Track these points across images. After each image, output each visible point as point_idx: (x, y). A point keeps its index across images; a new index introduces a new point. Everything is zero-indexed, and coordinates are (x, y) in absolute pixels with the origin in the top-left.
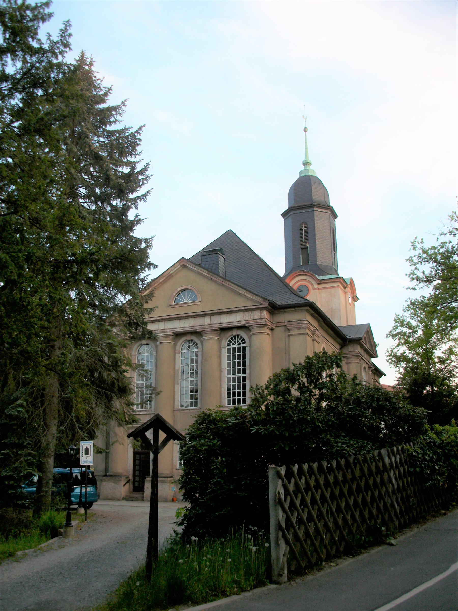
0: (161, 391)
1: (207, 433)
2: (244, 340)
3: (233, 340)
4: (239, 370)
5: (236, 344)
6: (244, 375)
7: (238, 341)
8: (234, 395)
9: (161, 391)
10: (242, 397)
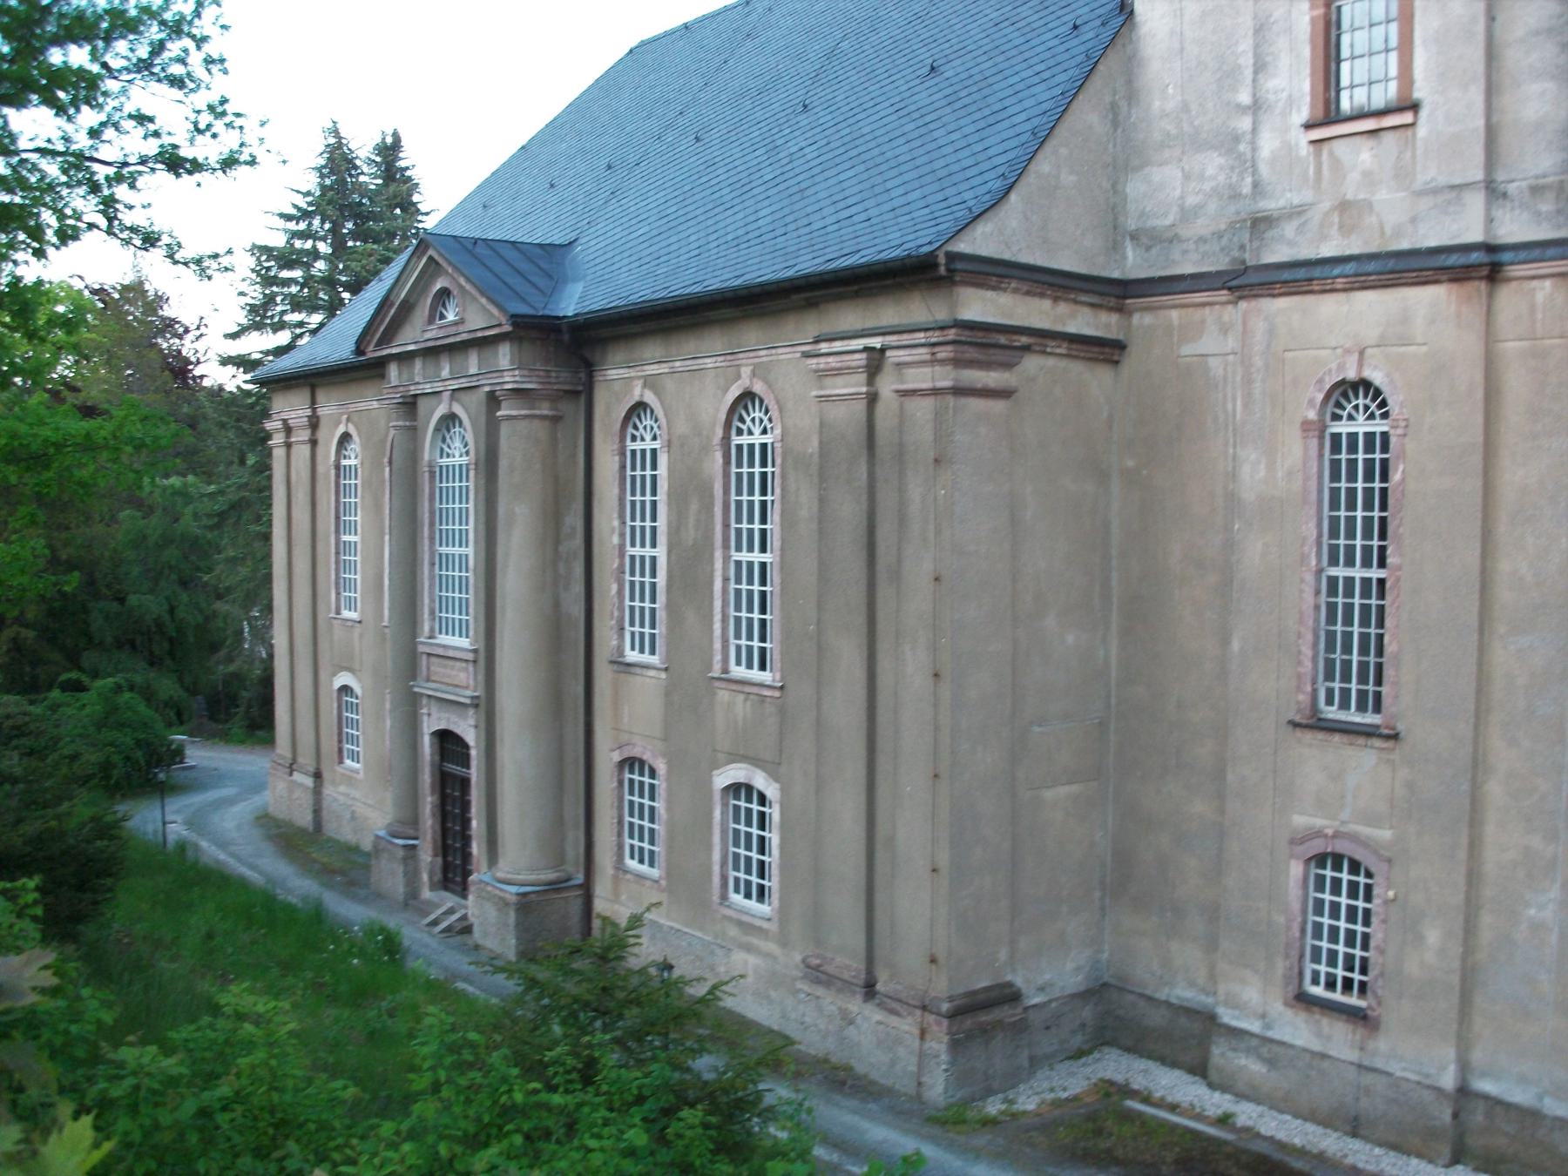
7: (1367, 408)
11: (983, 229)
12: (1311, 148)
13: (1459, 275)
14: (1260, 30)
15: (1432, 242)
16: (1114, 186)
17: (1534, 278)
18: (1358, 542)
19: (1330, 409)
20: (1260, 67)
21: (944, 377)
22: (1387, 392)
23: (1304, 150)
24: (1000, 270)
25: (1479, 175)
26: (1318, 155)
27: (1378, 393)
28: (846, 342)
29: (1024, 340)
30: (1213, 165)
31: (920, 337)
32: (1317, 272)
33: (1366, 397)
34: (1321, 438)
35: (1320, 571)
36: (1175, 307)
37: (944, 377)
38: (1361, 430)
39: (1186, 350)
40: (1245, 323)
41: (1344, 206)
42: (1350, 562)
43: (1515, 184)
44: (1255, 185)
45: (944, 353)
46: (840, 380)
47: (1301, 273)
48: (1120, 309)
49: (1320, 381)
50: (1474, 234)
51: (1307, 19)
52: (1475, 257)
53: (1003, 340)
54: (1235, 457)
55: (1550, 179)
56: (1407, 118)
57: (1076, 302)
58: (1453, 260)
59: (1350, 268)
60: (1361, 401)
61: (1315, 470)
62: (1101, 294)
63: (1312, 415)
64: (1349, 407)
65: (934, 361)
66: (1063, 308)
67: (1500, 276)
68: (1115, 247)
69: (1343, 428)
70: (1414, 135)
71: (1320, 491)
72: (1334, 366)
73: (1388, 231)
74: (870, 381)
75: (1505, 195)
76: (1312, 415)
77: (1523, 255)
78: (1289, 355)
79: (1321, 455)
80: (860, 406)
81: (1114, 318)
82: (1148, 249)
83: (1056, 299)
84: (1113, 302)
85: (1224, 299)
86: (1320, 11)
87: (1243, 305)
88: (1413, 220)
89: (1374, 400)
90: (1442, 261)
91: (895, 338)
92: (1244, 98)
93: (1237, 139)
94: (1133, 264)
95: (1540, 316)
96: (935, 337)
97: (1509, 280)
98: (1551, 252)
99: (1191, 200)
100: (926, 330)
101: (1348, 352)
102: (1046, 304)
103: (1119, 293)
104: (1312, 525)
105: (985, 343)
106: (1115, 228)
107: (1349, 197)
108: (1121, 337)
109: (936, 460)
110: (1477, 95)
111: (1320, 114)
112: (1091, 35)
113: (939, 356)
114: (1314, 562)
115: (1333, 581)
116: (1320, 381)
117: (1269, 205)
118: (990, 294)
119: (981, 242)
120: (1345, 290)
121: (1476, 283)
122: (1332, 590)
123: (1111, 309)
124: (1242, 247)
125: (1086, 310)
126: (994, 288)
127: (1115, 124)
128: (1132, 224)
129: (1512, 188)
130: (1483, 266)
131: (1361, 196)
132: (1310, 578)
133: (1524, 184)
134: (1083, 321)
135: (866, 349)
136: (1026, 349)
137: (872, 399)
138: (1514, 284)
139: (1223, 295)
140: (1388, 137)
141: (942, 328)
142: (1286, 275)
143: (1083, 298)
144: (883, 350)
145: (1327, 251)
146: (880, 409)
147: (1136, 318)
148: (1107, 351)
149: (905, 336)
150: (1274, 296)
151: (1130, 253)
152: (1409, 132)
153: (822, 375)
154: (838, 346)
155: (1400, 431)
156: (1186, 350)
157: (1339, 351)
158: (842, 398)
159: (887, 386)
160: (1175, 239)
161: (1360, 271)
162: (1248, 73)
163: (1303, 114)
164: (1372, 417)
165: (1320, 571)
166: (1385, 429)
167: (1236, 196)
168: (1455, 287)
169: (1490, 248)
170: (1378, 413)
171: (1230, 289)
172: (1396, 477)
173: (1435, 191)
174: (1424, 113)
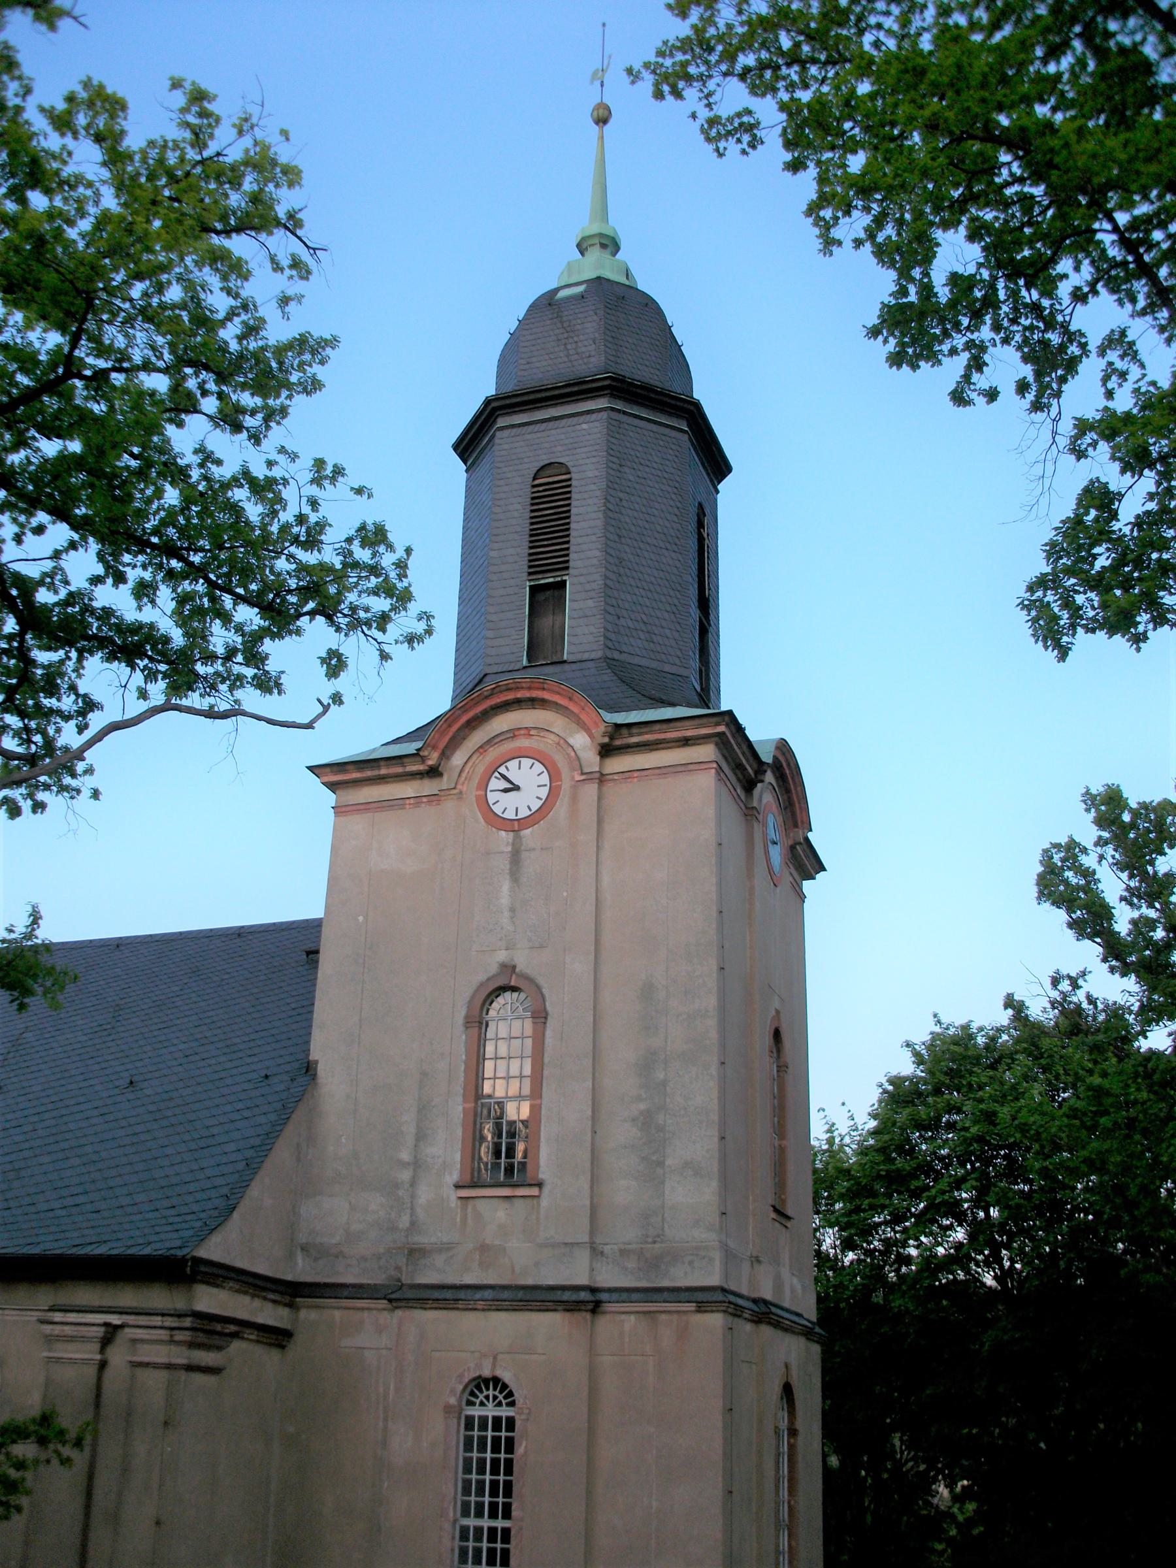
0: (1063, 653)
1: (195, 336)
2: (511, 1394)
3: (481, 1392)
4: (493, 1507)
5: (490, 1405)
6: (507, 1524)
7: (495, 1397)
8: (480, 1491)
9: (1063, 653)
10: (502, 1478)
11: (216, 1239)
12: (459, 1202)
13: (572, 1307)
14: (423, 1109)
15: (551, 1282)
16: (294, 1207)
17: (623, 1313)
18: (487, 1499)
19: (466, 1396)
20: (421, 1136)
21: (181, 1356)
22: (513, 1386)
23: (453, 1202)
24: (220, 1272)
25: (586, 1239)
26: (464, 1208)
27: (505, 1386)
28: (81, 1315)
29: (232, 1328)
30: (376, 1203)
31: (157, 1321)
32: (462, 1294)
33: (495, 1389)
34: (459, 1418)
35: (455, 1521)
36: (338, 1308)
37: (181, 1356)
38: (490, 1414)
39: (347, 1342)
40: (399, 1328)
41: (483, 1248)
42: (479, 1514)
43: (608, 1247)
44: (413, 1223)
45: (180, 1336)
46: (71, 1346)
47: (448, 1294)
48: (290, 1305)
49: (461, 1376)
50: (582, 1279)
51: (461, 1108)
52: (583, 1296)
53: (219, 1327)
54: (385, 1429)
55: (633, 1246)
56: (534, 1191)
57: (265, 1298)
58: (567, 1296)
59: (488, 1294)
60: (491, 1393)
61: (454, 1443)
62: (281, 1293)
63: (453, 1401)
64: (481, 1397)
65: (172, 1341)
66: (257, 1303)
67: (601, 1309)
68: (290, 1256)
69: (476, 1412)
70: (539, 1205)
71: (457, 1459)
72: (472, 1365)
73: (517, 1270)
74: (102, 1350)
75: (602, 1253)
76: (453, 1401)
77: (615, 1296)
78: (437, 1354)
79: (458, 1431)
80: (92, 1371)
81: (284, 1312)
82: (316, 1259)
83: (253, 1296)
84: (287, 1299)
85: (381, 1306)
86: (471, 1105)
87: (399, 1313)
88: (536, 1264)
89: (501, 1392)
90: (558, 1295)
91: (132, 1317)
92: (405, 1156)
93: (397, 1185)
94: (301, 1270)
95: (627, 1340)
96: (169, 1322)
97: (604, 1313)
98: (635, 1296)
99: (355, 1227)
100: (163, 1315)
101: (484, 1355)
102: (246, 1299)
103: (292, 1292)
104: (451, 1485)
105: (211, 1330)
106: (292, 1240)
107: (487, 1242)
108: (289, 1327)
109: (166, 1423)
110: (584, 1183)
111: (468, 1178)
112: (282, 1087)
113: (176, 1338)
114: (451, 1514)
115: (464, 1532)
116: (461, 1376)
117: (421, 1240)
118: (214, 1291)
119: (213, 1250)
120: (483, 1310)
121: (584, 1314)
122: (464, 1536)
123: (286, 1305)
124: (398, 1268)
125: (270, 1305)
126: (217, 1286)
127: (299, 1160)
128: (302, 1238)
129: (607, 1249)
130: (588, 1302)
131: (497, 1242)
132: (447, 1526)
133: (615, 1247)
134: (268, 1314)
135: (106, 1325)
136: (235, 1335)
137: (103, 1365)
138: (608, 1316)
139: (383, 1303)
140: (519, 1203)
141: (179, 1316)
142: (436, 1294)
143: (271, 1296)
144: (122, 1326)
145: (469, 1279)
146: (109, 1373)
147: (303, 1314)
148: (278, 1337)
149: (141, 1318)
150: (425, 1309)
151: (300, 1262)
152: (535, 1201)
153: (50, 1340)
154: (72, 1317)
155: (523, 1417)
156: (347, 1342)
157: (477, 1354)
158: (73, 1362)
159: (118, 1356)
160: (340, 1255)
161: (497, 1297)
162: (410, 1140)
163: (454, 1176)
164: (500, 1404)
165: (455, 1521)
166: (511, 1414)
167: (393, 1229)
168: (567, 1314)
169: (593, 1290)
170: (504, 1402)
171: (390, 1301)
172: (520, 1450)
173: (554, 1246)
174: (546, 1190)
